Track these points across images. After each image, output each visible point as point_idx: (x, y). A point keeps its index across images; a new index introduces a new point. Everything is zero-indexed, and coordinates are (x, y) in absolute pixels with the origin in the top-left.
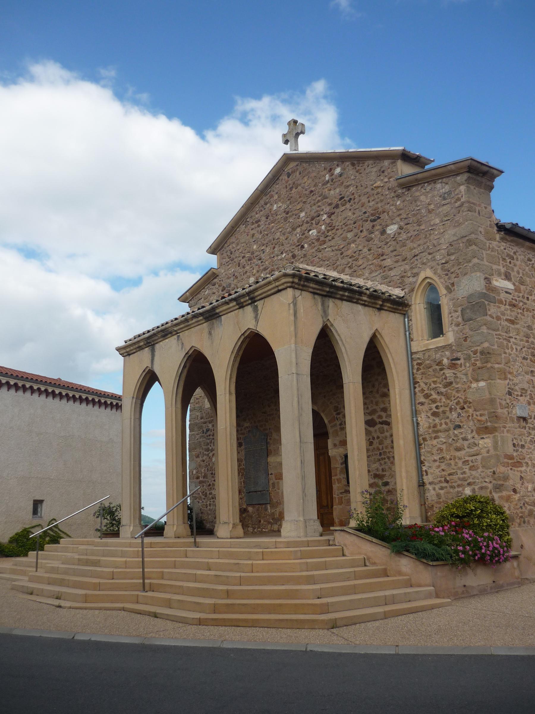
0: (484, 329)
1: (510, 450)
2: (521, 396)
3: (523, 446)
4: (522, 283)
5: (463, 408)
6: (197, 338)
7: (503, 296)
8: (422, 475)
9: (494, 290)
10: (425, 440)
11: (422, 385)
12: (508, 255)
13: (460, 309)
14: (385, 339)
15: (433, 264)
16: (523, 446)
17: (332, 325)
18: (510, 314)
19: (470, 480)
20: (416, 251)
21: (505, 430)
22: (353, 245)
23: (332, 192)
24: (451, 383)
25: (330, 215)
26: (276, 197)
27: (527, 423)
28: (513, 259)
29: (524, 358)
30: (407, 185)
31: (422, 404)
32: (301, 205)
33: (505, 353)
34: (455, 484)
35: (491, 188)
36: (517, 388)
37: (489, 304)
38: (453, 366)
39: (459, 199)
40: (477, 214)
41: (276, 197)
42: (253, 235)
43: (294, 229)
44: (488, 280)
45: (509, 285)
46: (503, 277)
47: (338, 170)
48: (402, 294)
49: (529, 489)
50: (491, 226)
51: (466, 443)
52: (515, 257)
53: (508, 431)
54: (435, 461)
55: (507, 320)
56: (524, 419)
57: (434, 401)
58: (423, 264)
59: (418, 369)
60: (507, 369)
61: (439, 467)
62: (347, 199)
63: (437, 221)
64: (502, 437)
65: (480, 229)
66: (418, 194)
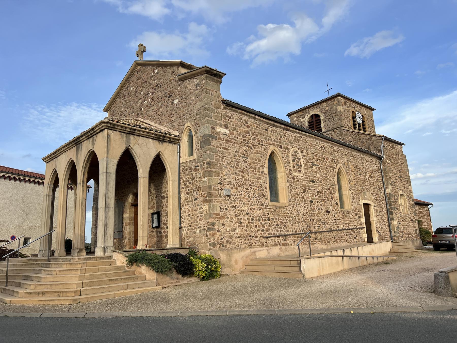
0: (208, 152)
1: (218, 211)
2: (228, 185)
3: (226, 209)
4: (234, 129)
5: (198, 190)
6: (71, 154)
7: (222, 136)
8: (181, 223)
9: (218, 133)
10: (183, 206)
11: (184, 179)
12: (227, 116)
13: (199, 142)
14: (165, 156)
15: (191, 119)
16: (226, 209)
17: (132, 148)
18: (225, 145)
19: (199, 226)
20: (185, 113)
21: (216, 201)
22: (161, 109)
23: (154, 82)
24: (194, 178)
25: (153, 93)
26: (132, 84)
27: (230, 198)
28: (231, 118)
29: (231, 167)
30: (183, 79)
31: (183, 188)
32: (142, 88)
33: (220, 164)
34: (193, 228)
35: (221, 82)
36: (225, 181)
37: (212, 140)
38: (196, 170)
39: (202, 87)
40: (210, 95)
41: (132, 84)
42: (122, 103)
43: (138, 100)
44: (213, 128)
45: (227, 131)
46: (223, 127)
47: (157, 71)
48: (177, 133)
49: (228, 230)
50: (218, 101)
51: (198, 207)
52: (232, 117)
53: (217, 202)
54: (186, 216)
55: (223, 148)
56: (229, 196)
57: (187, 187)
58: (187, 119)
59: (182, 171)
60: (221, 171)
61: (188, 219)
62: (159, 86)
63: (193, 98)
64: (213, 205)
65: (211, 103)
66: (186, 84)
